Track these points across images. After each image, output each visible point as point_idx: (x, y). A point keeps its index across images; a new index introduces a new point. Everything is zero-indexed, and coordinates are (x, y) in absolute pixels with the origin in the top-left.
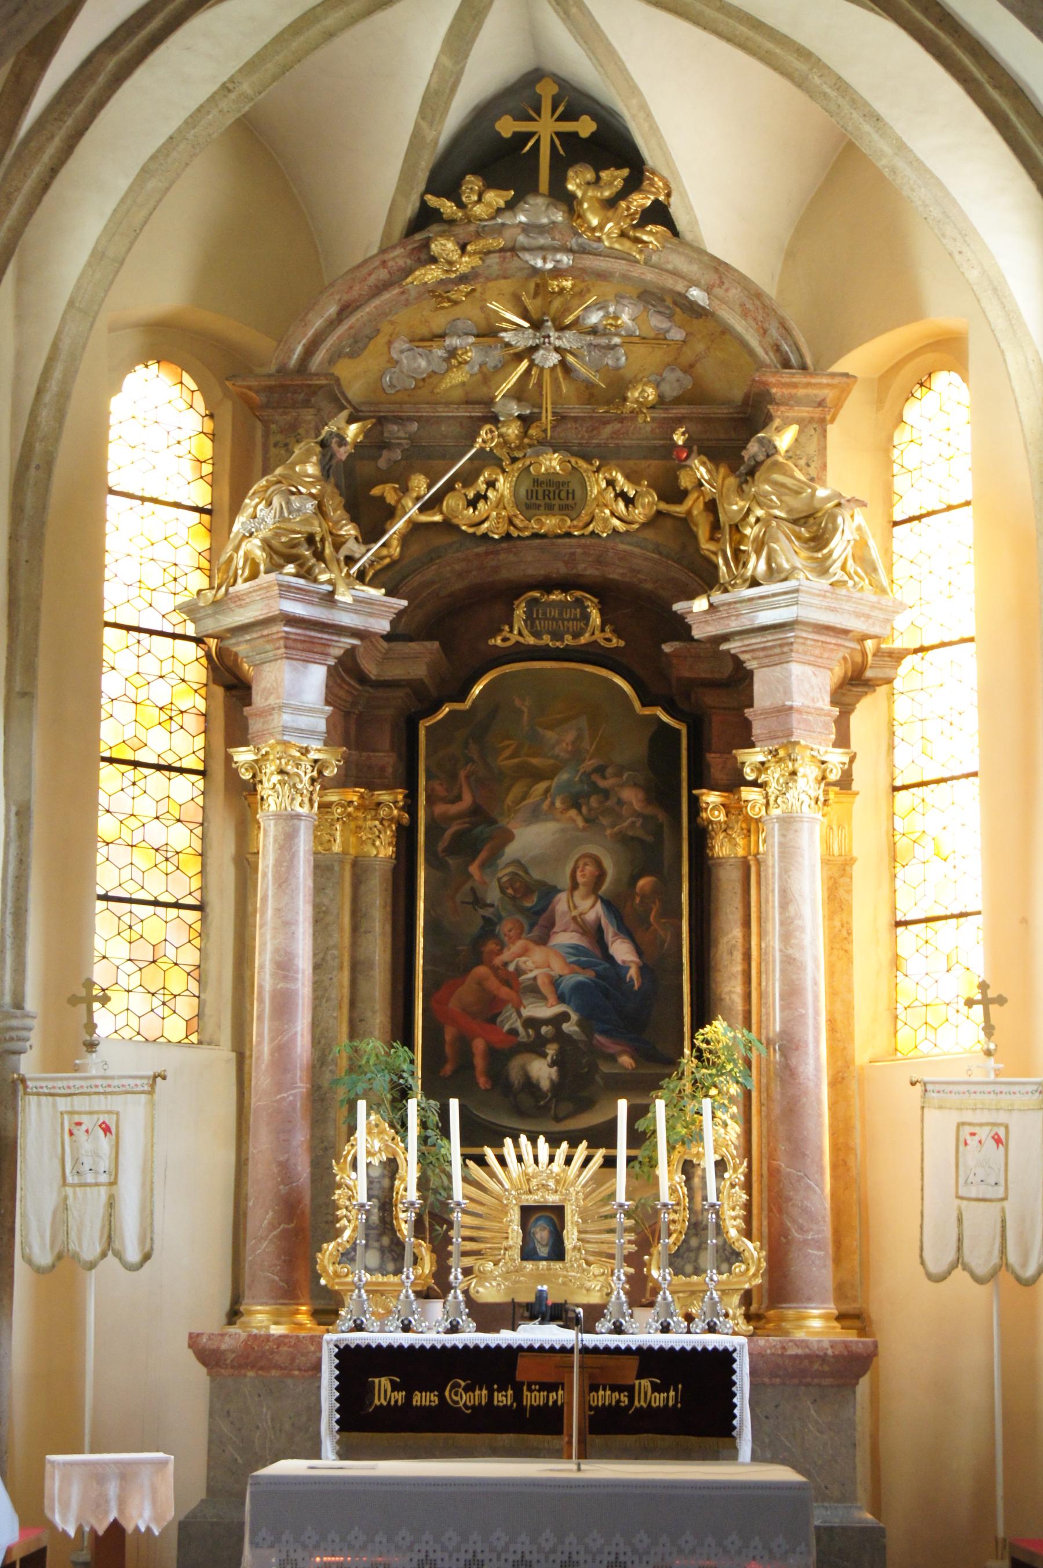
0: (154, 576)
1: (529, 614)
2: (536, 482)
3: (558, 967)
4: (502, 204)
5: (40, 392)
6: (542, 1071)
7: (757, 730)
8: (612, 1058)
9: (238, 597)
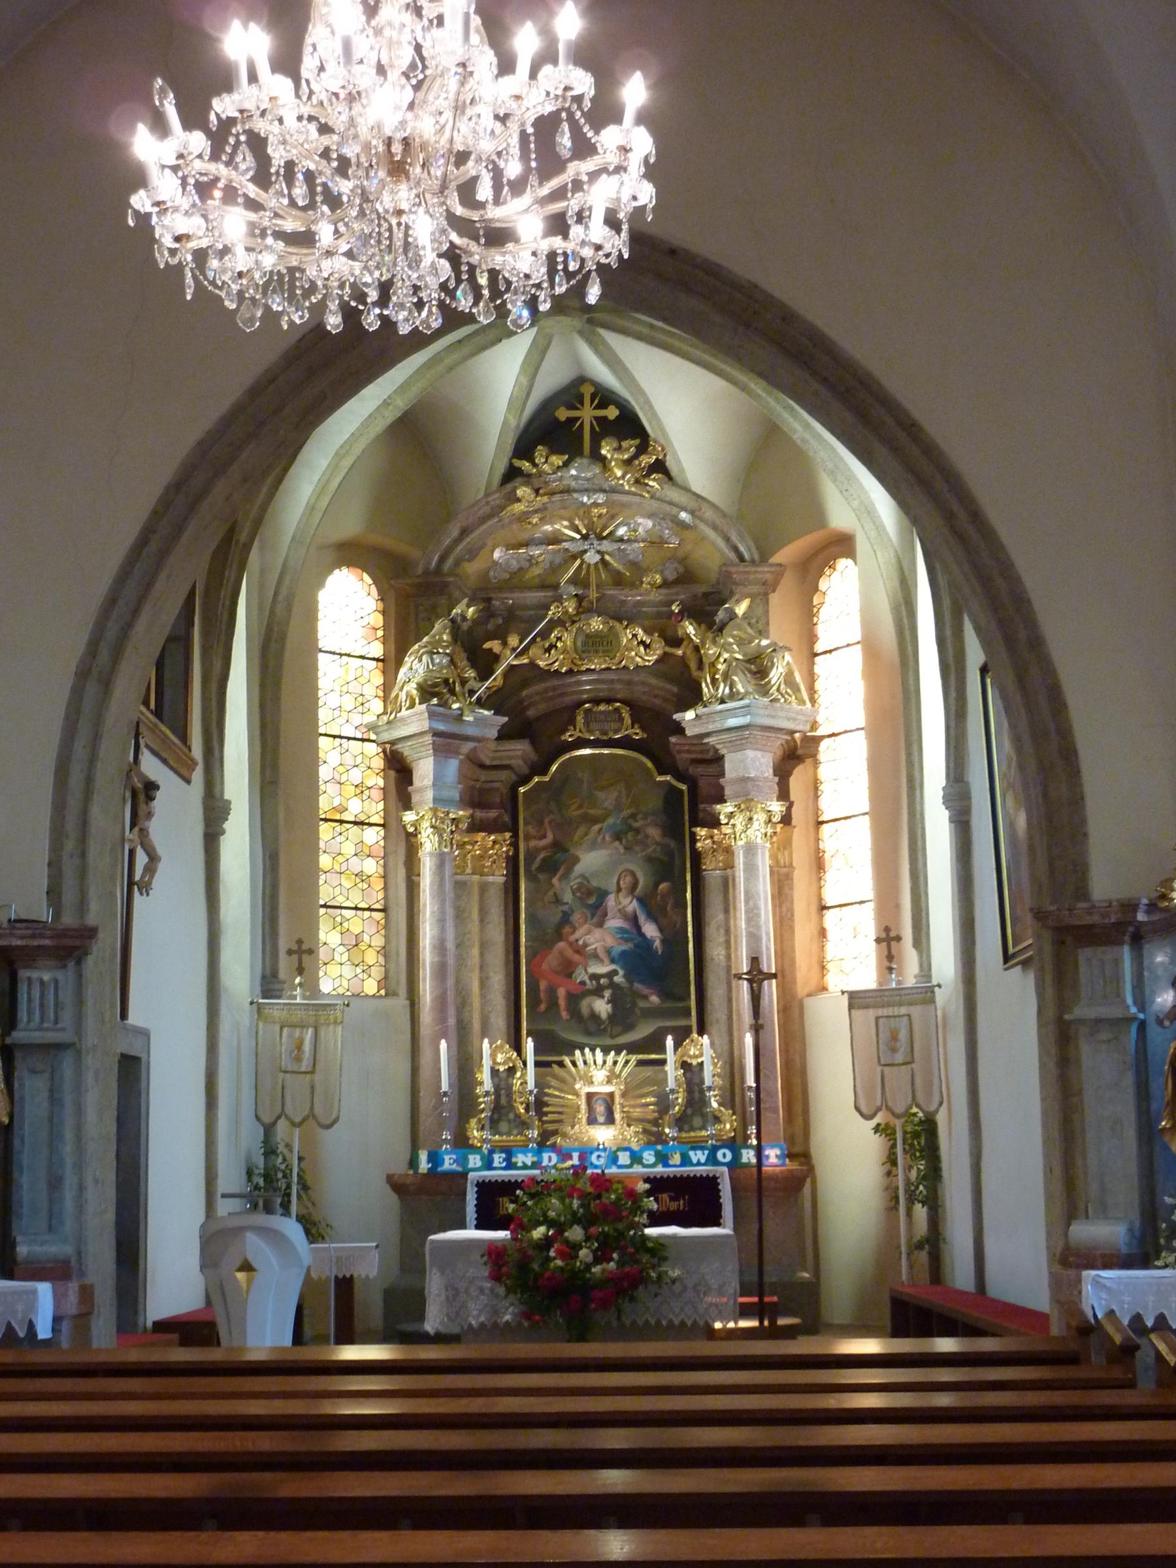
0: (349, 702)
1: (586, 718)
2: (587, 636)
3: (610, 941)
4: (561, 464)
5: (276, 594)
6: (602, 1007)
7: (727, 792)
8: (646, 997)
9: (403, 719)
